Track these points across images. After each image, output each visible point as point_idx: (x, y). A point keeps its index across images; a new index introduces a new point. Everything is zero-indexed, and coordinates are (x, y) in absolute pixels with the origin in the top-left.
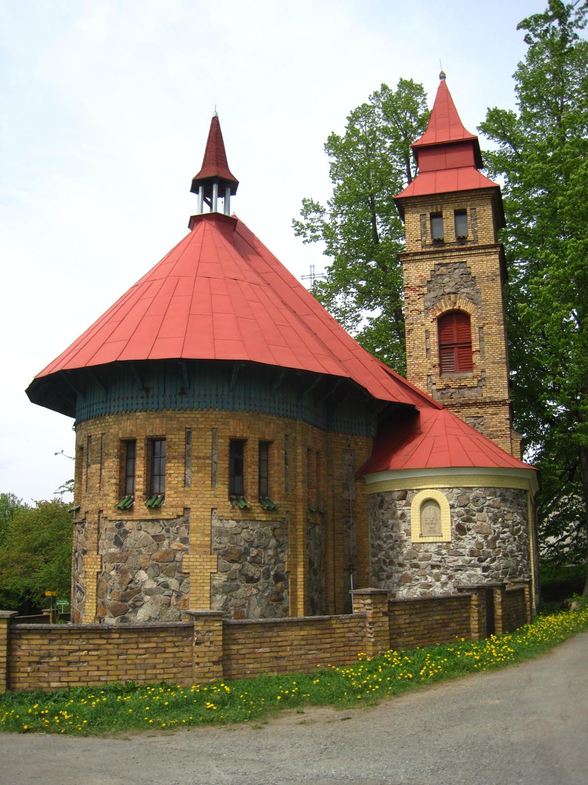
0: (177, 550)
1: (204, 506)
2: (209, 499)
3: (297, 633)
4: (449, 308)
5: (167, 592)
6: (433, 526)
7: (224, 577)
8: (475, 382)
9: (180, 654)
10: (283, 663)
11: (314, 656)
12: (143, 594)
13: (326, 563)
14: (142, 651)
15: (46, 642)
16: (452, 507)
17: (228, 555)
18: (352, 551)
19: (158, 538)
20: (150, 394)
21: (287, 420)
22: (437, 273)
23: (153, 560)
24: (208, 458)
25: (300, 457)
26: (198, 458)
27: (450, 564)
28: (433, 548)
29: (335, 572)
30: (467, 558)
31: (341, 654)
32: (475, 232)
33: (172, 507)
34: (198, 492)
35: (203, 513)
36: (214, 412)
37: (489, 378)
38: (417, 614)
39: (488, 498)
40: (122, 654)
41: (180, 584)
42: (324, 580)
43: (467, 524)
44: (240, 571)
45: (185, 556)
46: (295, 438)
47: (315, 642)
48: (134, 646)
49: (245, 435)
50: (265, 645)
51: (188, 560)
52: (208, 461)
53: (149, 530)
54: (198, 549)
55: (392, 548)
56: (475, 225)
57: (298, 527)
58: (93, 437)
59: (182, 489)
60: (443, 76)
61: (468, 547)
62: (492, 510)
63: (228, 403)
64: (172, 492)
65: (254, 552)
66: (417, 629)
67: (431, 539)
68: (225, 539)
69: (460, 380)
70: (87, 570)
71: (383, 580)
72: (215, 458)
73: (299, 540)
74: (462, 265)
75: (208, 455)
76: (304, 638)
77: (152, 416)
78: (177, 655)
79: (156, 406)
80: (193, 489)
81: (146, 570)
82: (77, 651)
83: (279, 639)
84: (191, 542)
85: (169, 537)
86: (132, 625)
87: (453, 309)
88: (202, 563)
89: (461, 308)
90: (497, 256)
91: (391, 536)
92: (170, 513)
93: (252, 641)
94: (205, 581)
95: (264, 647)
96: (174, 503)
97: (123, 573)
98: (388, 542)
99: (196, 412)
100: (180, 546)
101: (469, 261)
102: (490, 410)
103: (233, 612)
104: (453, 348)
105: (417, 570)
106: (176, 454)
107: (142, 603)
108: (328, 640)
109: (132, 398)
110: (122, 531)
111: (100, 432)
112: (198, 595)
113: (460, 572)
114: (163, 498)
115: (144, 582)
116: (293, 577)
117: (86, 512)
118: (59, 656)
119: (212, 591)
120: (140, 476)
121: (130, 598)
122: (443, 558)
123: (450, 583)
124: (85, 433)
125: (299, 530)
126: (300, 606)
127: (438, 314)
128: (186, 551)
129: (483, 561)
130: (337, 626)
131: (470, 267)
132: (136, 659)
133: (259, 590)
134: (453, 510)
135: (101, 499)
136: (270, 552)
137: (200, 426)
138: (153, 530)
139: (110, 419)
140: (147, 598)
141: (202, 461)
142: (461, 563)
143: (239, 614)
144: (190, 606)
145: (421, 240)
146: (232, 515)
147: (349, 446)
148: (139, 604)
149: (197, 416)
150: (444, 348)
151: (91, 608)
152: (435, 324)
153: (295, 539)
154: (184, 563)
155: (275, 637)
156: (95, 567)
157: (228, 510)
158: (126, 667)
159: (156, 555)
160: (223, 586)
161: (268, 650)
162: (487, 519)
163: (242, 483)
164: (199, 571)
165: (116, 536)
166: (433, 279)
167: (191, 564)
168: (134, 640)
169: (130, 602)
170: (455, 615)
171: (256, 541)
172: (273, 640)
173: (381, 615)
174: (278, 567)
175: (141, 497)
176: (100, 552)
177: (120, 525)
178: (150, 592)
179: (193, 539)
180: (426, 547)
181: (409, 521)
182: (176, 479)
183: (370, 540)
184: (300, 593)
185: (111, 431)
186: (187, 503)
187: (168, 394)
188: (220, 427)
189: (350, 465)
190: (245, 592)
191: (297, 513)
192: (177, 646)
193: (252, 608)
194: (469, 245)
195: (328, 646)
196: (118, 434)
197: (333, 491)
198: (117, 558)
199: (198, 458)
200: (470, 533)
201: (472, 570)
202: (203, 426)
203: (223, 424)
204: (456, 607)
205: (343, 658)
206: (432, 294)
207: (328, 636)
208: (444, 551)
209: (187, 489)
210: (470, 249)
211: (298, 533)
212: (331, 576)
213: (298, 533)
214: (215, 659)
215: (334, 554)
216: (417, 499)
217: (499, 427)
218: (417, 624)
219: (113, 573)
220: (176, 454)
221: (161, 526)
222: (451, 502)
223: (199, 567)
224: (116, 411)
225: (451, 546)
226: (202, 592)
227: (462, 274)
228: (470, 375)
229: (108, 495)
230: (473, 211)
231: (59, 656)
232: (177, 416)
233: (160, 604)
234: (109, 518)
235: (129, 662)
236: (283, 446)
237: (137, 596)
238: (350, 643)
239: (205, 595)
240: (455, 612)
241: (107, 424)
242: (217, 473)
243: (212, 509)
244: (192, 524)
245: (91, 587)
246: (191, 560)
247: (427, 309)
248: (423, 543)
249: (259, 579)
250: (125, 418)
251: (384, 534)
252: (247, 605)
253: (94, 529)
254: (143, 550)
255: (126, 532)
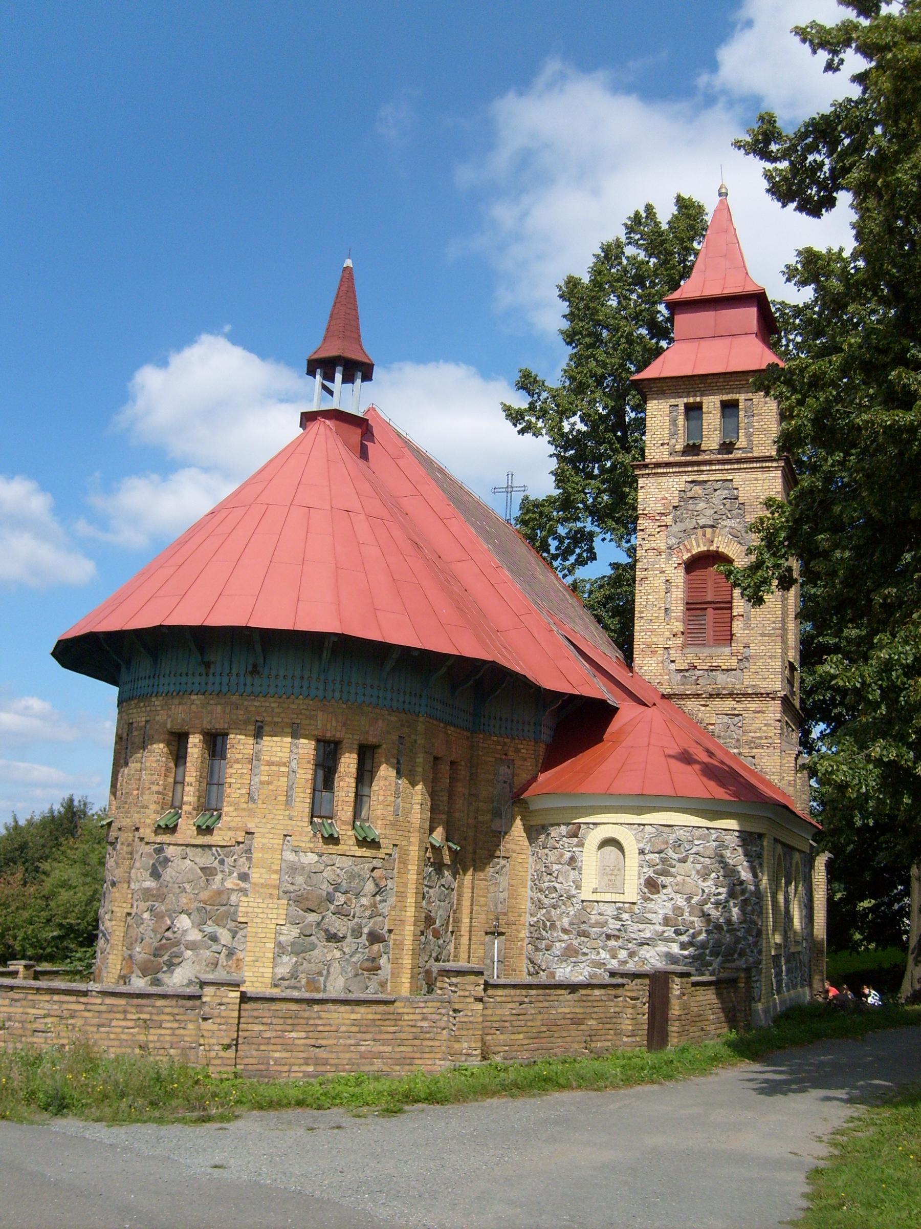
0: (233, 890)
1: (274, 831)
2: (281, 822)
3: (346, 1016)
4: (703, 548)
5: (215, 947)
6: (613, 877)
7: (295, 932)
8: (733, 663)
9: (182, 1032)
10: (322, 1054)
11: (369, 1048)
12: (183, 948)
13: (457, 921)
14: (131, 1024)
15: (7, 1002)
16: (642, 852)
17: (304, 902)
18: (500, 906)
19: (208, 872)
20: (211, 671)
21: (403, 716)
22: (690, 494)
23: (200, 902)
24: (284, 764)
25: (420, 769)
26: (270, 764)
27: (633, 935)
28: (610, 910)
29: (470, 935)
30: (660, 928)
31: (409, 1049)
32: (749, 436)
33: (230, 829)
34: (267, 811)
35: (271, 841)
36: (296, 701)
37: (757, 657)
38: (531, 1003)
39: (697, 842)
40: (103, 1025)
41: (234, 938)
42: (452, 945)
43: (662, 878)
44: (318, 924)
45: (243, 898)
46: (415, 742)
47: (371, 1029)
48: (121, 1016)
49: (338, 735)
50: (299, 1028)
51: (246, 904)
52: (283, 769)
53: (197, 860)
54: (262, 890)
55: (554, 907)
56: (750, 425)
57: (410, 867)
58: (135, 725)
59: (245, 806)
60: (723, 194)
61: (660, 911)
62: (702, 859)
63: (317, 688)
64: (231, 809)
65: (340, 899)
66: (529, 1024)
67: (608, 897)
68: (300, 879)
69: (712, 657)
70: (114, 909)
71: (541, 950)
72: (294, 764)
73: (410, 886)
74: (727, 484)
75: (284, 760)
76: (355, 1023)
77: (212, 702)
78: (177, 1032)
79: (217, 688)
80: (260, 806)
81: (189, 915)
82: (45, 1017)
83: (320, 1022)
84: (252, 880)
85: (223, 872)
86: (170, 991)
87: (708, 551)
88: (266, 911)
89: (720, 550)
90: (779, 473)
91: (555, 888)
92: (227, 838)
93: (281, 1021)
94: (268, 935)
95: (298, 1031)
96: (232, 824)
97: (158, 916)
98: (551, 896)
99: (272, 700)
100: (238, 885)
101: (737, 478)
102: (754, 706)
103: (304, 981)
104: (706, 609)
105: (586, 940)
106: (240, 756)
107: (181, 959)
108: (391, 1029)
109: (187, 675)
110: (161, 859)
111: (144, 719)
112: (257, 954)
113: (646, 947)
114: (220, 817)
115: (186, 931)
116: (398, 937)
117: (120, 829)
118: (22, 1022)
119: (277, 949)
120: (190, 784)
121: (166, 953)
122: (623, 925)
123: (630, 961)
124: (126, 717)
125: (412, 872)
126: (405, 979)
127: (686, 556)
128: (244, 892)
129: (681, 934)
130: (406, 1010)
131: (737, 489)
132: (122, 1033)
133: (344, 953)
134: (642, 857)
135: (138, 812)
136: (365, 901)
137: (276, 719)
138: (203, 860)
139: (157, 702)
140: (189, 953)
141: (274, 768)
142: (648, 935)
143: (312, 984)
144: (246, 968)
145: (668, 444)
146: (312, 845)
147: (506, 755)
148: (176, 961)
149: (273, 705)
150: (694, 607)
151: (115, 962)
152: (681, 572)
153: (405, 885)
154: (240, 909)
155: (314, 1019)
156: (125, 905)
157: (307, 839)
158: (106, 1043)
159: (204, 895)
160: (293, 944)
161: (303, 1035)
162: (694, 872)
163: (332, 801)
164: (260, 920)
165: (153, 865)
166: (682, 504)
167: (250, 910)
168: (120, 1009)
169: (166, 958)
170: (595, 1009)
171: (344, 883)
172: (311, 1022)
173: (472, 1000)
174: (375, 923)
175: (190, 813)
176: (132, 886)
177: (159, 851)
178: (192, 946)
179: (254, 875)
180: (603, 907)
181: (581, 869)
182: (238, 791)
183: (529, 891)
184: (407, 961)
185: (157, 718)
186: (251, 826)
187: (234, 671)
188: (304, 722)
189: (505, 782)
190: (324, 955)
191: (411, 848)
192: (177, 1021)
193: (332, 978)
194: (738, 454)
195: (390, 1036)
196: (166, 724)
197: (476, 818)
198: (153, 896)
199: (270, 764)
200: (664, 891)
201: (665, 946)
202: (280, 720)
203: (309, 718)
204: (598, 998)
205: (411, 1055)
206: (679, 527)
207: (393, 1023)
208: (625, 916)
209: (251, 805)
210: (739, 461)
211: (409, 876)
212: (465, 940)
213: (409, 876)
214: (226, 1041)
215: (472, 910)
216: (594, 837)
217: (764, 731)
218: (531, 1017)
219: (146, 916)
220: (240, 756)
221: (213, 855)
222: (641, 845)
223: (260, 915)
224: (166, 691)
225: (636, 909)
226: (263, 950)
227: (725, 498)
228: (727, 650)
229: (147, 807)
230: (749, 403)
231: (22, 1022)
232: (246, 703)
233: (204, 963)
234: (146, 840)
235: (112, 1036)
236: (395, 752)
237: (175, 949)
238: (422, 1036)
239: (267, 955)
240: (595, 1004)
241: (153, 708)
242: (294, 786)
243: (285, 836)
244: (256, 855)
245: (117, 933)
246: (251, 904)
247: (670, 548)
248: (597, 902)
249: (344, 937)
250: (176, 701)
251: (546, 884)
252: (325, 972)
253: (127, 853)
254: (187, 886)
255: (167, 860)
